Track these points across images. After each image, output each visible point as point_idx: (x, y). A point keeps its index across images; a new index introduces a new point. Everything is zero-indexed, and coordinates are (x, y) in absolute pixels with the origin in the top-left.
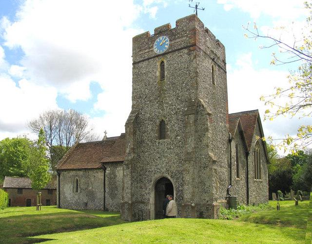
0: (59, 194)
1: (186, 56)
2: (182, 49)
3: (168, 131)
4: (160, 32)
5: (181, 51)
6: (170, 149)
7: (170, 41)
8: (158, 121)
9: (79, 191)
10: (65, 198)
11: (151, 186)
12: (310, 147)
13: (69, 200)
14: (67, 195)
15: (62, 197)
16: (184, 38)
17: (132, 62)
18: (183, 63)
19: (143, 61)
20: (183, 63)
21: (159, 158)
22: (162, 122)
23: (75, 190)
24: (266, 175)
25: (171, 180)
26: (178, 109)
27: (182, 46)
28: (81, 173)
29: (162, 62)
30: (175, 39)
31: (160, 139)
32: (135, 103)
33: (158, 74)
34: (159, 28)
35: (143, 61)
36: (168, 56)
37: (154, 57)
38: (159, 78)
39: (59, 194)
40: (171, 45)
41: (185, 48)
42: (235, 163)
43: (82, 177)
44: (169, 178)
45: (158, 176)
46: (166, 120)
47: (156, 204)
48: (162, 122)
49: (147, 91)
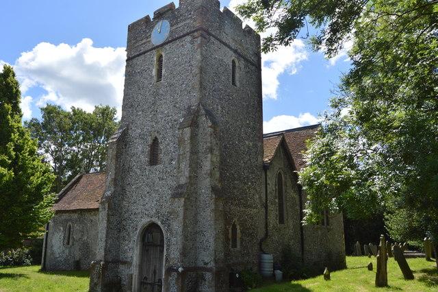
0: (46, 247)
1: (189, 45)
2: (184, 36)
3: (161, 153)
4: (160, 15)
5: (183, 39)
6: (163, 179)
7: (172, 26)
8: (150, 141)
9: (71, 243)
10: (53, 253)
11: (135, 237)
12: (2, 280)
13: (58, 256)
14: (55, 248)
15: (49, 251)
16: (188, 21)
17: (126, 58)
18: (184, 55)
19: (138, 55)
20: (184, 55)
21: (148, 193)
22: (155, 140)
23: (66, 241)
24: (168, 255)
25: (162, 227)
26: (175, 121)
27: (185, 32)
28: (75, 216)
29: (161, 56)
30: (177, 23)
31: (151, 165)
32: (125, 113)
33: (154, 72)
34: (157, 11)
35: (138, 55)
36: (167, 47)
37: (152, 49)
38: (155, 78)
39: (46, 247)
40: (171, 32)
41: (188, 34)
42: (277, 201)
43: (76, 221)
44: (159, 223)
45: (145, 221)
46: (160, 137)
47: (141, 267)
48: (155, 140)
49: (140, 97)
